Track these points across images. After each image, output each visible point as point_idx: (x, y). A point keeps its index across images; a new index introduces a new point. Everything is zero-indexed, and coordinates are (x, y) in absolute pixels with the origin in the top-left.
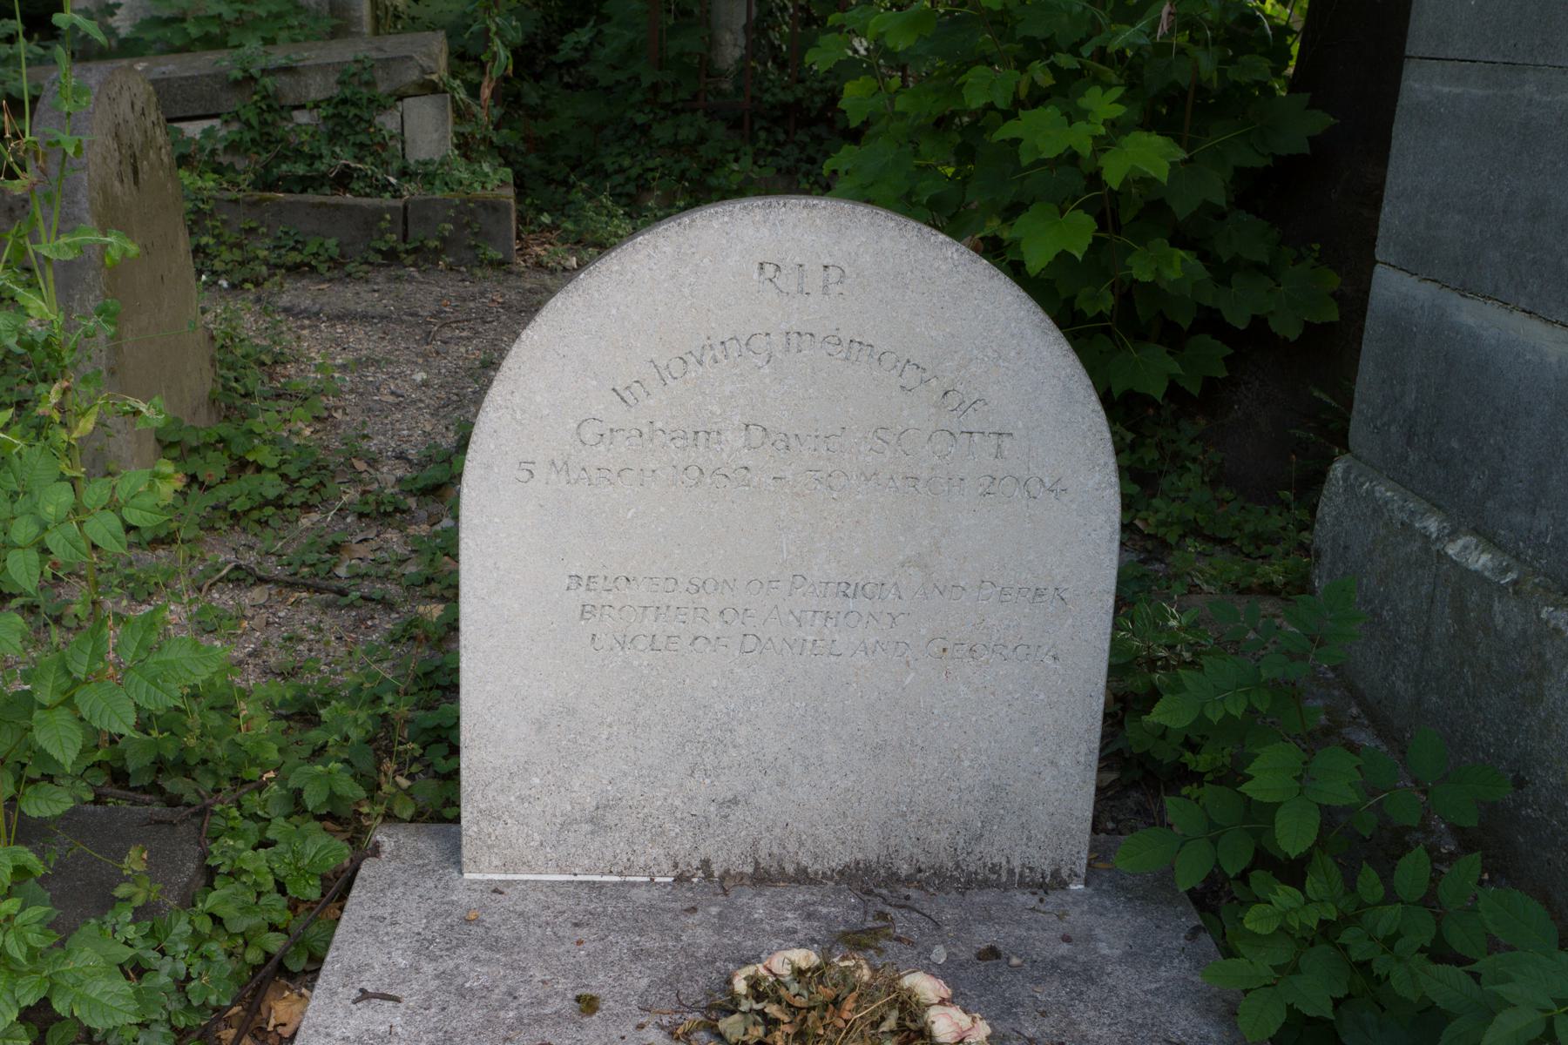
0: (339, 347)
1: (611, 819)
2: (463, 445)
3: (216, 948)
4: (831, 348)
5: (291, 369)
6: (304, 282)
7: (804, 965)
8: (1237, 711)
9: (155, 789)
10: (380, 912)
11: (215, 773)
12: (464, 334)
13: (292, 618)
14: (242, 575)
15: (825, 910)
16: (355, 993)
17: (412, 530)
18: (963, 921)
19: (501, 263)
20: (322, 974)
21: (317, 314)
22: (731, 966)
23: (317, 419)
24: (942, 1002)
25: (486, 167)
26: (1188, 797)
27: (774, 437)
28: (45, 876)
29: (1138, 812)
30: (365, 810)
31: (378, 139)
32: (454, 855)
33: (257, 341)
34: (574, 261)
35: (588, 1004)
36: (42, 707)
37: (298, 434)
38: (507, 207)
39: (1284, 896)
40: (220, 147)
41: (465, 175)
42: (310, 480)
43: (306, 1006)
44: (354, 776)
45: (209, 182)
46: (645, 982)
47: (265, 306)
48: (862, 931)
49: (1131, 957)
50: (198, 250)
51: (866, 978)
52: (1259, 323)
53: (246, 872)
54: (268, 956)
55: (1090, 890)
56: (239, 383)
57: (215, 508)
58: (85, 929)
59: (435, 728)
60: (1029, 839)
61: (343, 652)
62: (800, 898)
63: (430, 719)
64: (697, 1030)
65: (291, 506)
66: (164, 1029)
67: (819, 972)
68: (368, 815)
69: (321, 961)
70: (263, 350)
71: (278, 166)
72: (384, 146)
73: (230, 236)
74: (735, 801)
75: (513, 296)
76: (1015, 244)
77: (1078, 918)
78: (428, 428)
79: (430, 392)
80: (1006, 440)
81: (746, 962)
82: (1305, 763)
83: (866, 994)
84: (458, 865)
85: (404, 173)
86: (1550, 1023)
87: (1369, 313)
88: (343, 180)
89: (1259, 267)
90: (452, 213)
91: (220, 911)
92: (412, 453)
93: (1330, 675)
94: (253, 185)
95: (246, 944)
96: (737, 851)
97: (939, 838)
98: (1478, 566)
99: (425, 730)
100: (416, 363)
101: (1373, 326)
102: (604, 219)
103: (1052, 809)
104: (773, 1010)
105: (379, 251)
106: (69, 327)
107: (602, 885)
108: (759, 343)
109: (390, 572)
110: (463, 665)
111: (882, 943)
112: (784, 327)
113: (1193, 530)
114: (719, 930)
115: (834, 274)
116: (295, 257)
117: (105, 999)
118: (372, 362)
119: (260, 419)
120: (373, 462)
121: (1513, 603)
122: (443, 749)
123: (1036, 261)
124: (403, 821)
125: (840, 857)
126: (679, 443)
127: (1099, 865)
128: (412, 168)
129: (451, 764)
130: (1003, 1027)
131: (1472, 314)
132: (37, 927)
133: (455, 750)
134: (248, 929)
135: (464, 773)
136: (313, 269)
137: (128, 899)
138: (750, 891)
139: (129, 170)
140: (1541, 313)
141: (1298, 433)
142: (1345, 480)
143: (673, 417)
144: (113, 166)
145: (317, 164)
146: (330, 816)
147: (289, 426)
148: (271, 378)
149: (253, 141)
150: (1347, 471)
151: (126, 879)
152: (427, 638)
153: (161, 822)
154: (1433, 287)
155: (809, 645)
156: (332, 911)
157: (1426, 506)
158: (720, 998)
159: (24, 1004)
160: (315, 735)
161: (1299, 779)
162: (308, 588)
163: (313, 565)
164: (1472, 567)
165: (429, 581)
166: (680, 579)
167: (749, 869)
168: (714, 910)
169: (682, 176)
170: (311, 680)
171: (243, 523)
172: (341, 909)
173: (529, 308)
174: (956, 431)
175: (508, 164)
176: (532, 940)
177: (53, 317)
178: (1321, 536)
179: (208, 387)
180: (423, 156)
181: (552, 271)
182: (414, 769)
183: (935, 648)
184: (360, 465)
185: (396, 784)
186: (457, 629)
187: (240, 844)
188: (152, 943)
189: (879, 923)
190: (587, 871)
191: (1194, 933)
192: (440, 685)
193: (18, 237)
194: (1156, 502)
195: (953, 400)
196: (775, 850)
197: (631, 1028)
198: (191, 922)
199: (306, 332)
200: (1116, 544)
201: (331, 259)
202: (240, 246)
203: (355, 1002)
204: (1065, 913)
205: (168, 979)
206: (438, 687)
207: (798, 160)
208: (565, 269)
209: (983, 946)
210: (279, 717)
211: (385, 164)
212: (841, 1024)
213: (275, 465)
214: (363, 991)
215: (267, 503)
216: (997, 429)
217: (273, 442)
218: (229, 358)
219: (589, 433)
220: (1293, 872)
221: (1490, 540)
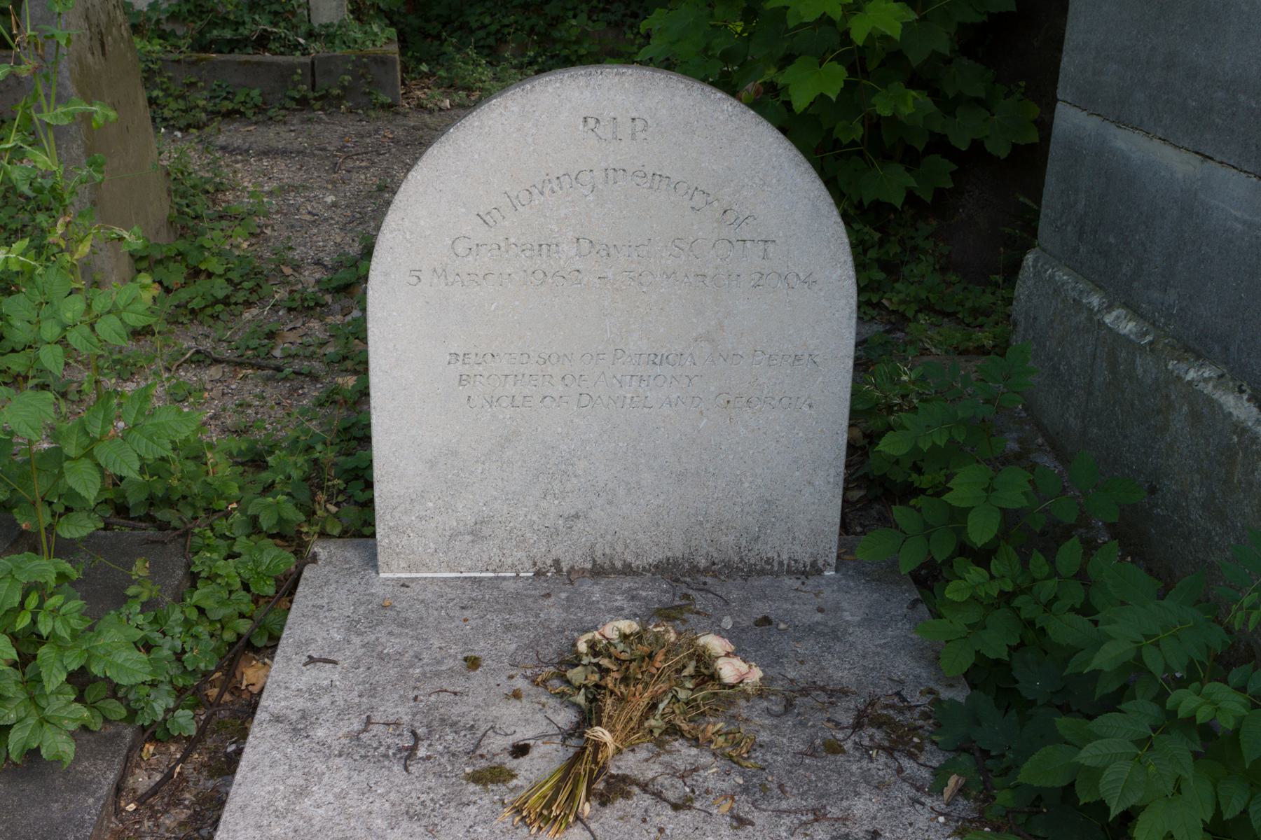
0: (268, 177)
1: (486, 531)
2: (368, 252)
3: (202, 630)
4: (639, 180)
5: (229, 196)
6: (236, 125)
7: (628, 631)
8: (941, 441)
9: (149, 518)
10: (319, 602)
11: (193, 506)
12: (363, 164)
13: (242, 389)
14: (201, 357)
15: (644, 594)
16: (304, 659)
17: (329, 320)
18: (746, 599)
19: (390, 106)
20: (280, 646)
21: (247, 151)
22: (576, 634)
23: (252, 234)
24: (728, 655)
25: (375, 28)
26: (914, 507)
27: (598, 247)
28: (79, 580)
29: (879, 520)
30: (305, 529)
31: (289, 7)
32: (372, 561)
33: (201, 174)
34: (447, 103)
35: (473, 663)
36: (68, 458)
37: (238, 247)
38: (394, 61)
39: (975, 574)
40: (163, 17)
41: (359, 35)
42: (250, 283)
43: (269, 671)
44: (296, 505)
45: (156, 46)
46: (513, 646)
47: (206, 145)
48: (672, 608)
49: (867, 622)
50: (152, 102)
51: (673, 639)
52: (977, 145)
53: (220, 576)
54: (239, 636)
55: (839, 575)
56: (191, 210)
57: (177, 307)
58: (107, 617)
59: (353, 469)
60: (794, 539)
61: (279, 413)
62: (626, 585)
63: (350, 463)
64: (552, 678)
65: (236, 304)
66: (168, 688)
67: (639, 637)
68: (307, 533)
69: (279, 638)
70: (208, 181)
71: (210, 32)
72: (294, 13)
73: (175, 89)
74: (577, 516)
75: (400, 133)
76: (785, 87)
77: (829, 595)
78: (338, 240)
79: (339, 211)
80: (771, 247)
81: (586, 631)
82: (991, 479)
83: (672, 650)
84: (375, 567)
85: (310, 35)
86: (1139, 649)
87: (1052, 140)
88: (262, 41)
89: (978, 102)
90: (350, 67)
91: (203, 604)
92: (327, 260)
93: (1023, 414)
94: (191, 47)
95: (223, 628)
96: (580, 553)
97: (728, 540)
98: (1126, 331)
99: (346, 471)
100: (327, 188)
101: (1055, 150)
102: (471, 67)
103: (810, 517)
104: (605, 662)
105: (293, 99)
106: (67, 174)
107: (481, 580)
108: (586, 177)
109: (314, 353)
110: (374, 421)
111: (686, 616)
112: (604, 165)
113: (926, 307)
114: (567, 610)
115: (640, 124)
116: (228, 105)
117: (127, 665)
118: (294, 188)
119: (208, 236)
120: (297, 268)
121: (1149, 358)
122: (361, 484)
123: (801, 101)
124: (334, 537)
125: (655, 555)
126: (528, 253)
127: (847, 557)
128: (317, 30)
129: (366, 495)
130: (773, 672)
131: (1126, 142)
132: (77, 615)
133: (369, 485)
134: (225, 616)
135: (377, 500)
136: (242, 114)
137: (136, 597)
138: (589, 581)
139: (97, 45)
140: (1171, 140)
141: (1007, 230)
142: (1035, 267)
143: (523, 234)
144: (86, 42)
145: (241, 30)
146: (279, 536)
147: (230, 241)
148: (214, 204)
149: (189, 11)
150: (1036, 260)
151: (133, 582)
152: (346, 402)
153: (153, 542)
154: (1098, 119)
155: (628, 401)
156: (284, 603)
157: (1091, 286)
158: (568, 657)
159: (70, 669)
160: (266, 476)
161: (986, 490)
162: (252, 366)
163: (255, 349)
164: (1122, 332)
165: (345, 358)
166: (532, 354)
167: (589, 566)
168: (563, 595)
169: (532, 30)
170: (259, 435)
171: (200, 317)
172: (291, 602)
173: (416, 145)
174: (733, 240)
175: (392, 24)
176: (431, 619)
177: (55, 168)
178: (1018, 309)
179: (167, 213)
180: (325, 21)
181: (431, 111)
182: (340, 498)
183: (721, 400)
184: (288, 271)
185: (327, 510)
186: (368, 395)
187: (215, 556)
188: (156, 627)
189: (684, 602)
190: (470, 570)
191: (914, 604)
192: (358, 436)
193: (26, 108)
194: (898, 286)
195: (730, 216)
196: (608, 551)
197: (504, 678)
198: (183, 612)
199: (239, 166)
200: (854, 321)
201: (256, 106)
202: (183, 97)
203: (305, 665)
204: (820, 592)
205: (170, 652)
206: (355, 438)
207: (624, 15)
208: (441, 109)
209: (760, 616)
210: (236, 464)
211: (295, 27)
212: (654, 671)
213: (222, 272)
214: (310, 657)
215: (217, 302)
216: (763, 237)
217: (219, 254)
218: (182, 188)
219: (461, 248)
220: (982, 557)
221: (1135, 311)
